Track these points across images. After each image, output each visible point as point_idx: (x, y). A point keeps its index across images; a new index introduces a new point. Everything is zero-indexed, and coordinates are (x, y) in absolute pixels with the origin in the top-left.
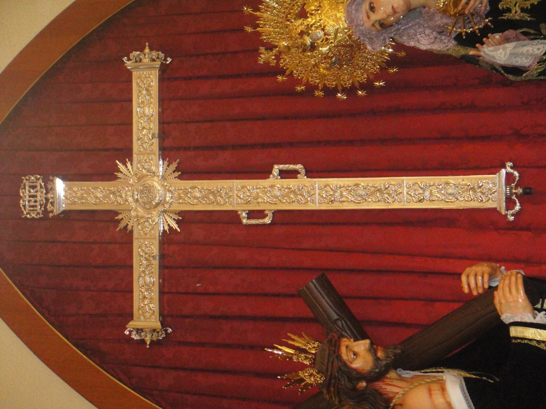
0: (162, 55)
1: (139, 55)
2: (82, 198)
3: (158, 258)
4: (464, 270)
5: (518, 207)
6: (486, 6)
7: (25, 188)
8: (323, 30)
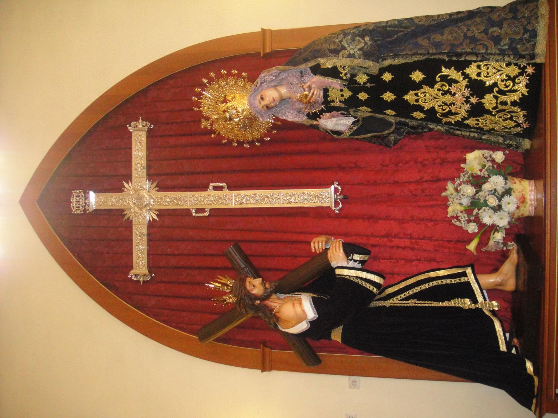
0: (148, 123)
1: (136, 123)
2: (104, 202)
3: (146, 235)
4: (312, 240)
5: (340, 206)
6: (321, 98)
7: (73, 197)
8: (236, 109)
